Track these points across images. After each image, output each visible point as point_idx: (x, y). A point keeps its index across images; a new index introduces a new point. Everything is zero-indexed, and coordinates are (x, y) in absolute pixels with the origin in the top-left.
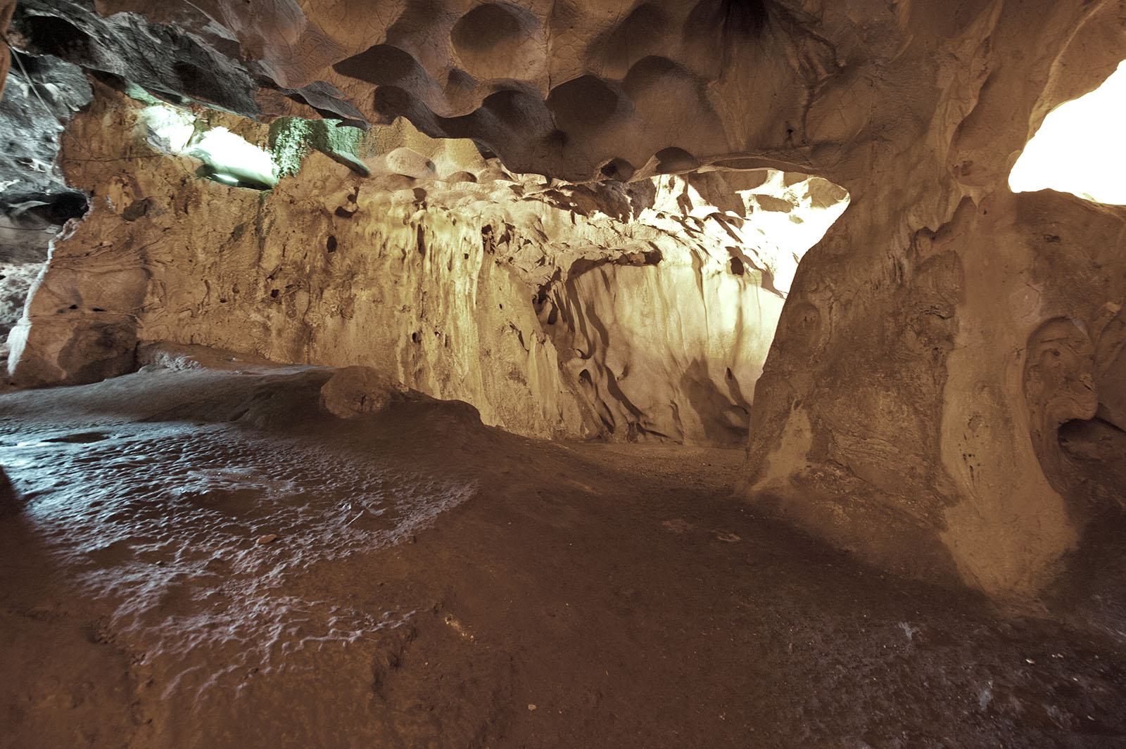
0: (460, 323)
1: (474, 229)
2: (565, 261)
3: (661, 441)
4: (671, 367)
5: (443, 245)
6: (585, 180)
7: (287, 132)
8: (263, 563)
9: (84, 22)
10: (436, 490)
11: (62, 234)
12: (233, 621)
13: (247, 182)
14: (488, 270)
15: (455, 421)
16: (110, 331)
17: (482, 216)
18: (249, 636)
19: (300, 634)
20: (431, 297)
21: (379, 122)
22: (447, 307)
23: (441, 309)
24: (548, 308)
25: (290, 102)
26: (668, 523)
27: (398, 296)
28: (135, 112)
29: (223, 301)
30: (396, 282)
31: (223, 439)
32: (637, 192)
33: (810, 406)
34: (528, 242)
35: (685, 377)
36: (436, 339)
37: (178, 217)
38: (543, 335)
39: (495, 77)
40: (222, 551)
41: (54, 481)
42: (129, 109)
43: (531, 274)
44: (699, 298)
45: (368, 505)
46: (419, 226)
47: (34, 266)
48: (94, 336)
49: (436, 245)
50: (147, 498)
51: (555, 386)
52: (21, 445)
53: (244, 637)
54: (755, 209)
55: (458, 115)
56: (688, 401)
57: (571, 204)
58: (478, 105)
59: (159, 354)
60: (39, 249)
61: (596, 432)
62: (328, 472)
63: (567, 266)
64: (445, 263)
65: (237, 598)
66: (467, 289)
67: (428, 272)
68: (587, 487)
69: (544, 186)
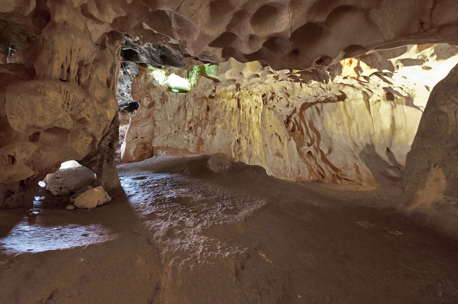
0: (255, 134)
1: (259, 96)
2: (298, 104)
3: (350, 183)
4: (354, 148)
5: (247, 104)
6: (307, 68)
7: (192, 71)
8: (195, 223)
9: (136, 49)
10: (251, 201)
11: (133, 115)
12: (187, 243)
13: (182, 91)
14: (265, 112)
15: (256, 173)
16: (146, 144)
17: (262, 90)
18: (193, 249)
19: (209, 250)
20: (243, 125)
21: (224, 61)
22: (249, 128)
23: (247, 129)
24: (291, 125)
25: (194, 60)
26: (359, 222)
27: (231, 126)
28: (149, 74)
29: (176, 132)
30: (230, 120)
31: (178, 179)
32: (332, 69)
33: (444, 166)
34: (281, 98)
35: (362, 153)
36: (246, 141)
37: (162, 106)
38: (289, 137)
39: (267, 34)
40: (182, 218)
41: (135, 192)
42: (148, 73)
43: (283, 112)
44: (368, 114)
45: (227, 205)
46: (238, 98)
47: (126, 126)
48: (142, 146)
49: (244, 104)
50: (159, 198)
51: (296, 158)
52: (126, 180)
53: (191, 249)
54: (400, 67)
55: (254, 52)
56: (364, 165)
57: (300, 80)
58: (261, 46)
59: (159, 151)
60: (127, 120)
61: (316, 178)
62: (212, 192)
63: (299, 106)
64: (248, 111)
65: (188, 235)
66: (257, 120)
67: (242, 115)
68: (315, 203)
69: (288, 74)
